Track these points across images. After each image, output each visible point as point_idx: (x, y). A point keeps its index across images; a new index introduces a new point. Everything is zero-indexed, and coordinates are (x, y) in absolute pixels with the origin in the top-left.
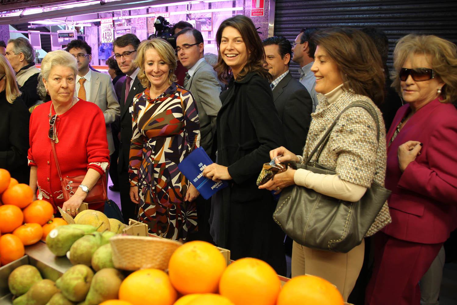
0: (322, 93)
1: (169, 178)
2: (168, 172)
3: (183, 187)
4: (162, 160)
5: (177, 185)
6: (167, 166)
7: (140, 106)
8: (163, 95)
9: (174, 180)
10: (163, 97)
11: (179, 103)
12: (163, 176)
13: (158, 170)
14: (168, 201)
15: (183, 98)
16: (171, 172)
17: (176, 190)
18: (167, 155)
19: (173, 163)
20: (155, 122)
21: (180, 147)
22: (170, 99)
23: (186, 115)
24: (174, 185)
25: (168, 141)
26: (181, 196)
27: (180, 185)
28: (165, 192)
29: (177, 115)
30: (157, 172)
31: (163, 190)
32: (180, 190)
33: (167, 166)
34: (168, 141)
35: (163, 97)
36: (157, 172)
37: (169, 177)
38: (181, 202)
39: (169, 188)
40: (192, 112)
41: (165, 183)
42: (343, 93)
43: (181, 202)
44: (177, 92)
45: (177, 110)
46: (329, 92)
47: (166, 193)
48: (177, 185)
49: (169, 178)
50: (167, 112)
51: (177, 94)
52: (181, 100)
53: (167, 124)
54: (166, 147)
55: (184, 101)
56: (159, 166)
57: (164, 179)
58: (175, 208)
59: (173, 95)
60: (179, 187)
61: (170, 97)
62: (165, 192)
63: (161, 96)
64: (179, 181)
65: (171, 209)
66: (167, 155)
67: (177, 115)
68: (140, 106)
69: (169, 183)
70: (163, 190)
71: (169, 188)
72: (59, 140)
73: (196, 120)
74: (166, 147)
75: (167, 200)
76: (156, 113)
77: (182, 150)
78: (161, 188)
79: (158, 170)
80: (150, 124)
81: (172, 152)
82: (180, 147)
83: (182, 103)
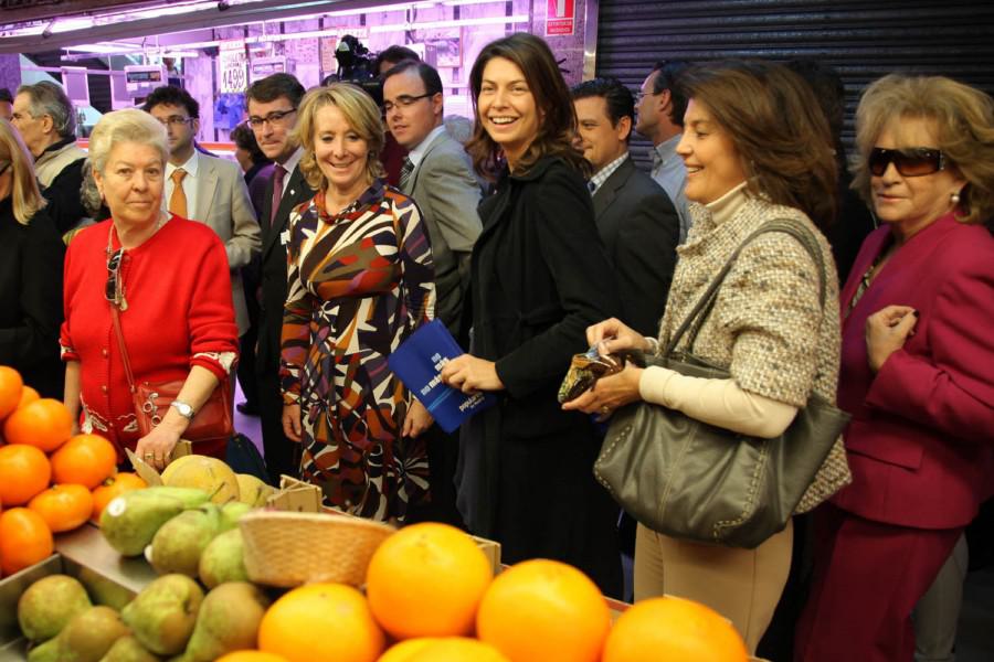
4: (353, 347)
6: (363, 361)
9: (378, 392)
10: (354, 210)
11: (390, 224)
14: (366, 437)
15: (398, 213)
16: (371, 374)
17: (383, 411)
18: (363, 335)
19: (376, 355)
20: (337, 264)
21: (391, 320)
22: (369, 214)
23: (404, 249)
24: (378, 402)
25: (366, 307)
26: (394, 426)
27: (391, 401)
28: (358, 416)
29: (385, 250)
30: (341, 374)
31: (355, 412)
32: (393, 412)
33: (363, 361)
34: (366, 307)
35: (354, 210)
36: (341, 374)
39: (369, 407)
40: (418, 242)
45: (385, 239)
49: (367, 387)
51: (385, 205)
52: (395, 217)
55: (401, 218)
56: (346, 360)
57: (356, 388)
60: (389, 406)
62: (358, 416)
64: (389, 392)
66: (363, 335)
67: (385, 250)
69: (367, 397)
70: (355, 412)
71: (369, 407)
76: (340, 245)
78: (349, 407)
79: (343, 368)
80: (327, 270)
82: (391, 320)
83: (395, 224)
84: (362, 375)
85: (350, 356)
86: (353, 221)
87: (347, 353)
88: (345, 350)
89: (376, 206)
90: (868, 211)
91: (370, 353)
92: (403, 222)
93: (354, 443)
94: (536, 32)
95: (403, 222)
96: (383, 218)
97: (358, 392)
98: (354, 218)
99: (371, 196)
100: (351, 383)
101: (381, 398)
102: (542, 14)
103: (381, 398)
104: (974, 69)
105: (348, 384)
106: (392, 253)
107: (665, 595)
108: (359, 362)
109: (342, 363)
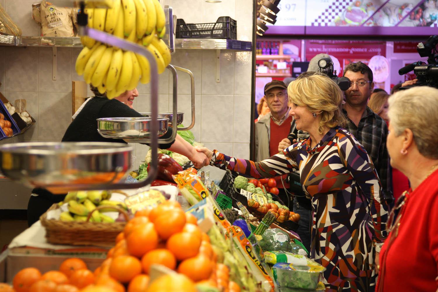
0: (269, 209)
1: (338, 245)
2: (337, 237)
3: (356, 256)
4: (328, 222)
5: (349, 253)
6: (334, 230)
7: (301, 155)
8: (320, 144)
9: (345, 248)
10: (319, 146)
11: (336, 151)
12: (330, 243)
13: (324, 235)
14: (339, 277)
15: (340, 144)
16: (339, 238)
17: (349, 260)
18: (332, 215)
19: (341, 226)
20: (313, 176)
21: (348, 205)
22: (327, 147)
23: (348, 165)
24: (345, 254)
25: (331, 200)
26: (355, 268)
27: (352, 253)
28: (334, 265)
29: (334, 167)
30: (323, 239)
31: (332, 263)
32: (354, 260)
33: (334, 230)
34: (331, 200)
35: (319, 146)
36: (323, 239)
37: (339, 244)
38: (356, 277)
39: (340, 258)
40: (355, 160)
41: (333, 253)
42: (289, 144)
43: (356, 277)
44: (335, 138)
45: (334, 160)
46: (366, 169)
47: (335, 267)
48: (349, 253)
49: (338, 245)
50: (325, 164)
51: (335, 141)
52: (338, 147)
53: (323, 179)
54: (330, 206)
55: (341, 147)
56: (325, 230)
57: (332, 246)
58: (350, 287)
59: (331, 142)
60: (351, 256)
61: (327, 144)
62: (334, 265)
63: (317, 146)
64: (351, 248)
65: (344, 288)
66: (332, 215)
67: (334, 167)
68: (301, 155)
69: (338, 252)
70: (332, 263)
71: (340, 258)
72: (336, 170)
73: (364, 168)
74: (330, 206)
75: (338, 276)
76: (316, 164)
77: (352, 208)
78: (328, 260)
79: (324, 235)
80: (310, 179)
81: (338, 211)
82: (348, 205)
83: (339, 151)
84: (334, 238)
85: (327, 227)
86: (320, 151)
87: (325, 226)
88: (324, 224)
89: (331, 142)
90: (387, 162)
91: (337, 225)
92: (343, 150)
93: (332, 284)
94: (375, 85)
95: (343, 150)
96: (334, 148)
97: (333, 250)
98: (320, 150)
99: (328, 137)
100: (329, 244)
101: (347, 251)
102: (379, 69)
103: (347, 251)
104: (288, 192)
105: (327, 244)
106: (340, 168)
107: (296, 162)
108: (343, 288)
109: (324, 232)
